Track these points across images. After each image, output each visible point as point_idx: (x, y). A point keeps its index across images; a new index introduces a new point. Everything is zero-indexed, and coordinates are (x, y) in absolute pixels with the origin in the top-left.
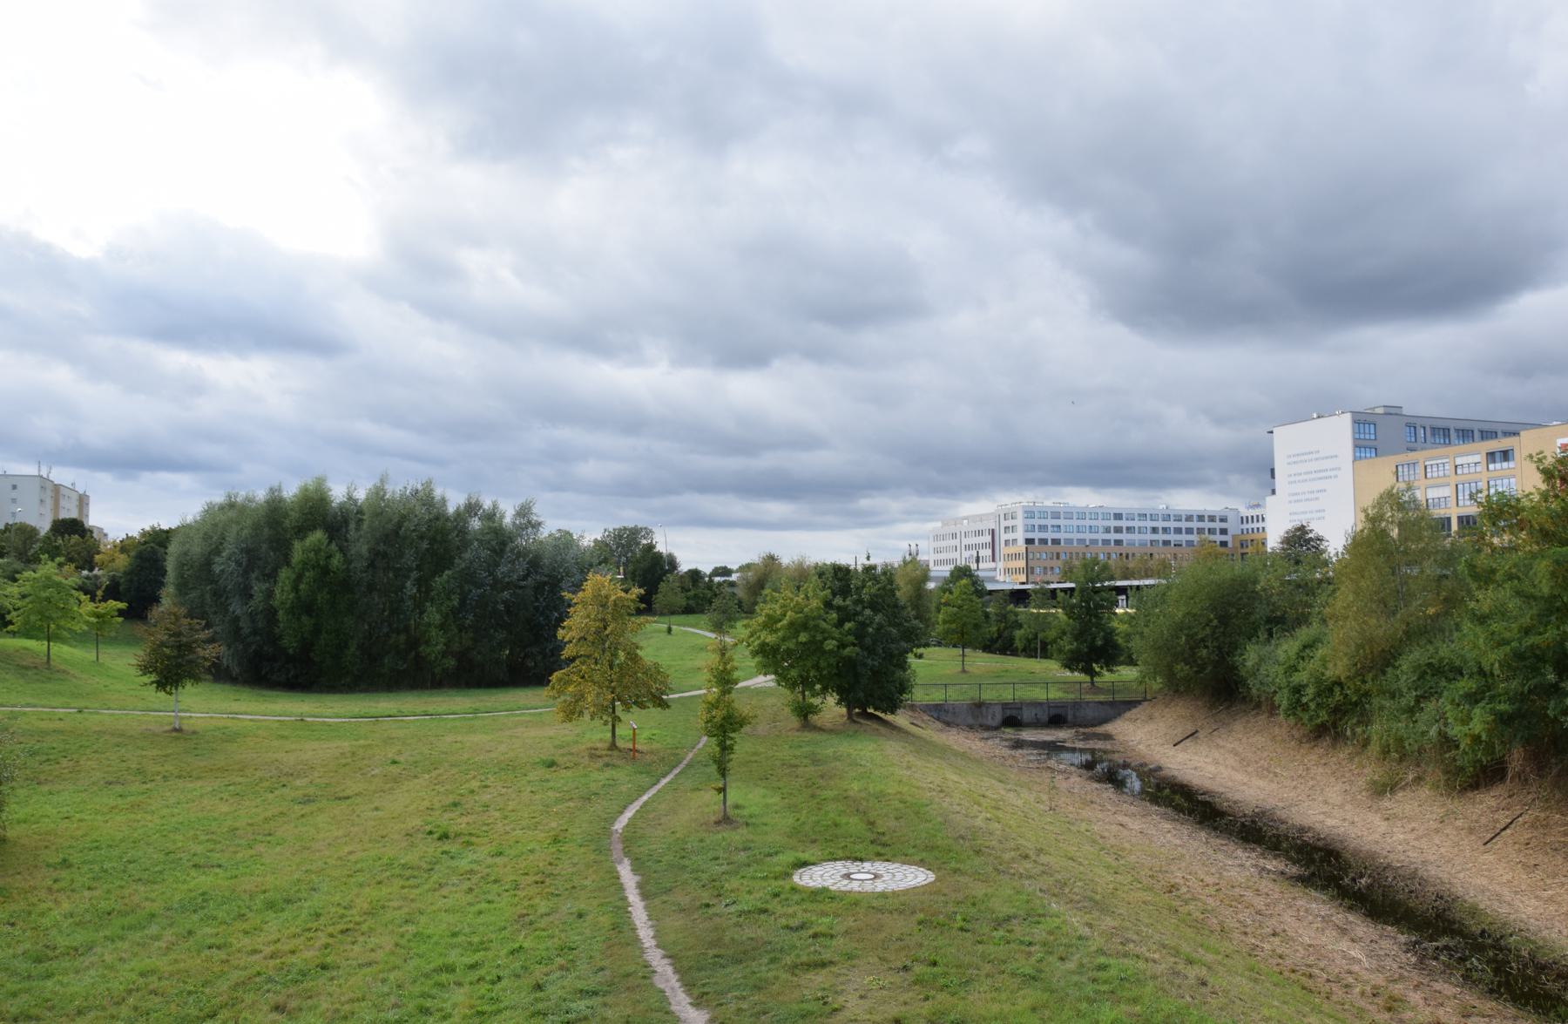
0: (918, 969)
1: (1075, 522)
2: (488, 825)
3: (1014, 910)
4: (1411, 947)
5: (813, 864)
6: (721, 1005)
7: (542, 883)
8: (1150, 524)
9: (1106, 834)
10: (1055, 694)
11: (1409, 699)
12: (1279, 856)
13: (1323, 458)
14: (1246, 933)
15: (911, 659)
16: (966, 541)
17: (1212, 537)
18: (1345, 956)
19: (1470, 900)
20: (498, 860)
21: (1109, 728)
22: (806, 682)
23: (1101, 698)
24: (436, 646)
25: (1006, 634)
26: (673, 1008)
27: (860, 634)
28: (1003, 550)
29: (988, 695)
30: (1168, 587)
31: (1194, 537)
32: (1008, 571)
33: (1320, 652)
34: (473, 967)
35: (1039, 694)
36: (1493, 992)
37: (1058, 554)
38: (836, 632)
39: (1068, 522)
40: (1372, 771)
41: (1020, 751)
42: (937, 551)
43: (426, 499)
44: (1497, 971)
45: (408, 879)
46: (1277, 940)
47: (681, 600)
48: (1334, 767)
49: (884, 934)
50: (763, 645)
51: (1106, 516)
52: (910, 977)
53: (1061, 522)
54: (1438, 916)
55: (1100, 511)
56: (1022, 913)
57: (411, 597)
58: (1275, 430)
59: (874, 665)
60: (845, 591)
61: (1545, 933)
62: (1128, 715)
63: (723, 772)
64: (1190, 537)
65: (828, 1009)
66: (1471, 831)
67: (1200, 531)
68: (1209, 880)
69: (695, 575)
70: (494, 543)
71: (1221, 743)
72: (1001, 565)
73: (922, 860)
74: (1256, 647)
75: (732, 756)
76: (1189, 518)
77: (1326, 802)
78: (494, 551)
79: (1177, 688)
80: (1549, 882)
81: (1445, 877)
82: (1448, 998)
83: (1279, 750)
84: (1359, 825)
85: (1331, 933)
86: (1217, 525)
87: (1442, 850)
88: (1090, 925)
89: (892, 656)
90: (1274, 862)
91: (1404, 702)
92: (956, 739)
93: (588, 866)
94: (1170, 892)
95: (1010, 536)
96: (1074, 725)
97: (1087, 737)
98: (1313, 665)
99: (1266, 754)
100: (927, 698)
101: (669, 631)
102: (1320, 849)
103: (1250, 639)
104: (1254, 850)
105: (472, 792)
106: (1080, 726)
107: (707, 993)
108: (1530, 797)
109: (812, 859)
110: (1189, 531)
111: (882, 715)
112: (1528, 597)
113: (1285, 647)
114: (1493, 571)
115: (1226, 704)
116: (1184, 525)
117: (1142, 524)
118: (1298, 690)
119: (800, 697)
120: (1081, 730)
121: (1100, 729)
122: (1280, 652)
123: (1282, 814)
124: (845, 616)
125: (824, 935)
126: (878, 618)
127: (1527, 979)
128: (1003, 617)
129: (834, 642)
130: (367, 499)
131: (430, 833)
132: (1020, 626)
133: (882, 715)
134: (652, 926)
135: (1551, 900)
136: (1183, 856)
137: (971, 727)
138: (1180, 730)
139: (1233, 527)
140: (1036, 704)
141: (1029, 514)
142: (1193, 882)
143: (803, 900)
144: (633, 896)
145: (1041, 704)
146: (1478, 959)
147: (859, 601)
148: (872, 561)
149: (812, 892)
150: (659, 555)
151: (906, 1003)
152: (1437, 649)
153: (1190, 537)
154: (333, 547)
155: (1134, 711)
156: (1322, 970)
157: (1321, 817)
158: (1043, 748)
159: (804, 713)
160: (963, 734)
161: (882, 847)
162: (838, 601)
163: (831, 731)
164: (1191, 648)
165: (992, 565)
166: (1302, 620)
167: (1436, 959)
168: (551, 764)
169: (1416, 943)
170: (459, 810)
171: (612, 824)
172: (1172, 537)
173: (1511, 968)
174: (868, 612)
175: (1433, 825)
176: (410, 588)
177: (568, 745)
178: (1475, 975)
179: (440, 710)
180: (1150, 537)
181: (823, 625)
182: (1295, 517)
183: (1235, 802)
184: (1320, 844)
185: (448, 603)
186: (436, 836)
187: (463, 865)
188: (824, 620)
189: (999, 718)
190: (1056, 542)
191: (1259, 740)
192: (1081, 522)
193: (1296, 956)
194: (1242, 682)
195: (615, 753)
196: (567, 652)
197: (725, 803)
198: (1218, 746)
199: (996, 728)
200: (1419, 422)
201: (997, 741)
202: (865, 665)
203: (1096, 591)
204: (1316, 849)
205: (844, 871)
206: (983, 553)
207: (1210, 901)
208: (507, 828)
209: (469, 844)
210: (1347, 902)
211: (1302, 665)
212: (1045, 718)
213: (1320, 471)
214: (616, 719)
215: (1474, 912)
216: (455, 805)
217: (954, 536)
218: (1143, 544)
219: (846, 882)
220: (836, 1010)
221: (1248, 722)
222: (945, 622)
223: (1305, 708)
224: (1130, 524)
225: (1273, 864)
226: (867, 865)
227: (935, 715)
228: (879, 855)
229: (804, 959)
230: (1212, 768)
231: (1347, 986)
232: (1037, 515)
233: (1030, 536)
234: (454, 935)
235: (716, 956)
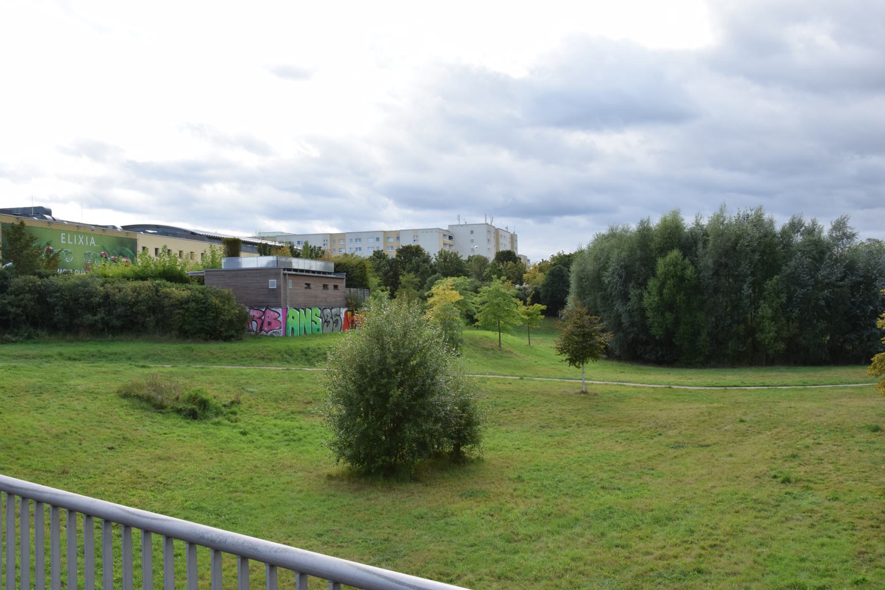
24: (769, 332)
57: (749, 296)
131: (775, 477)
154: (687, 261)
176: (747, 290)
185: (777, 300)
186: (779, 480)
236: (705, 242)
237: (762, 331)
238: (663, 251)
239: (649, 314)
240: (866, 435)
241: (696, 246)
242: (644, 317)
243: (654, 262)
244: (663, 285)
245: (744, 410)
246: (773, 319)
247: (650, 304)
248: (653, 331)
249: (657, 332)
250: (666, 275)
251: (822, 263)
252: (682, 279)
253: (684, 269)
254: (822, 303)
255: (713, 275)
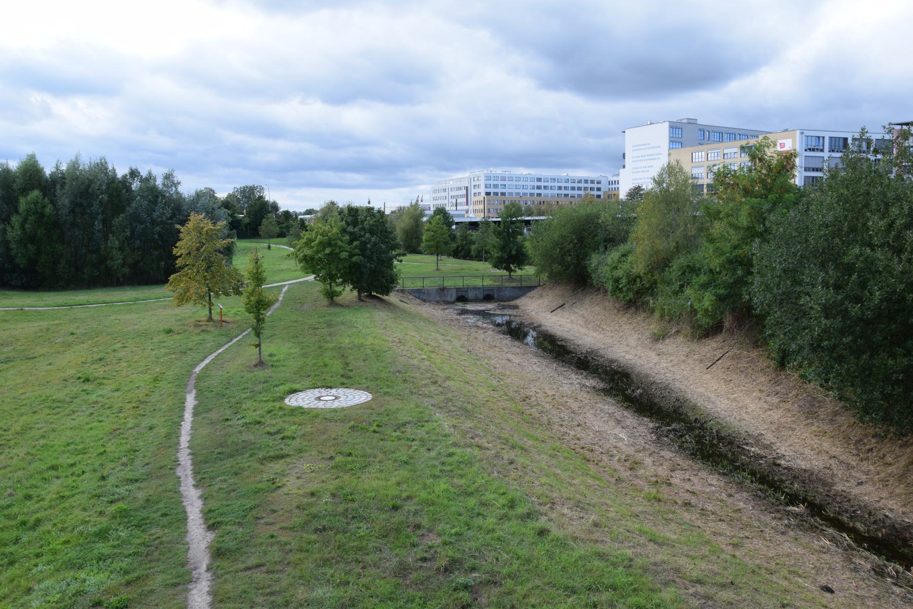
0: (339, 458)
1: (515, 183)
2: (117, 371)
3: (410, 418)
4: (655, 430)
5: (300, 391)
6: (210, 486)
7: (138, 407)
8: (557, 184)
9: (497, 366)
10: (487, 283)
11: (676, 287)
12: (595, 377)
13: (652, 148)
14: (562, 425)
15: (395, 262)
16: (451, 194)
17: (592, 193)
18: (616, 437)
19: (694, 401)
20: (116, 394)
21: (517, 302)
22: (332, 277)
23: (514, 284)
24: (117, 259)
25: (466, 248)
26: (181, 489)
27: (363, 248)
28: (473, 199)
29: (448, 283)
30: (553, 220)
31: (582, 192)
32: (475, 211)
33: (630, 258)
34: (72, 465)
35: (478, 283)
36: (693, 455)
37: (504, 201)
38: (348, 247)
39: (510, 183)
40: (654, 327)
41: (463, 316)
42: (435, 199)
43: (102, 167)
44: (697, 442)
45: (54, 409)
46: (579, 429)
47: (277, 230)
48: (635, 325)
49: (326, 436)
50: (305, 256)
51: (532, 180)
52: (331, 464)
53: (506, 183)
54: (674, 411)
55: (529, 176)
56: (414, 420)
57: (99, 231)
58: (626, 131)
59: (371, 268)
60: (355, 223)
61: (728, 418)
62: (529, 294)
63: (258, 334)
64: (580, 192)
65: (274, 486)
66: (701, 361)
67: (586, 189)
68: (550, 393)
69: (287, 214)
70: (150, 197)
71: (577, 311)
72: (471, 207)
73: (368, 387)
74: (597, 255)
75: (263, 325)
76: (580, 182)
77: (628, 345)
78: (150, 201)
79: (556, 279)
80: (735, 389)
81: (683, 387)
82: (666, 460)
83: (607, 315)
84: (643, 358)
85: (612, 423)
86: (595, 186)
87: (685, 372)
88: (454, 427)
89: (383, 261)
90: (591, 381)
91: (673, 287)
92: (427, 310)
93: (169, 396)
94: (525, 400)
95: (477, 191)
96: (500, 300)
97: (504, 307)
98: (625, 266)
99: (599, 317)
100: (413, 285)
101: (269, 247)
102: (620, 373)
103: (594, 251)
104: (581, 374)
105: (114, 351)
106: (501, 301)
107: (205, 478)
108: (734, 342)
109: (301, 388)
110: (579, 189)
111: (381, 296)
112: (736, 228)
113: (612, 256)
114: (719, 212)
115: (581, 289)
116: (576, 185)
117: (553, 184)
118: (617, 280)
119: (328, 287)
120: (502, 303)
121: (512, 303)
122: (609, 259)
123: (602, 352)
124: (354, 237)
125: (288, 437)
126: (373, 239)
127: (712, 445)
128: (465, 237)
129: (347, 253)
130: (68, 170)
131: (79, 378)
132: (474, 243)
133: (381, 296)
134: (191, 434)
135: (735, 400)
136: (539, 378)
137: (438, 302)
138: (555, 303)
139: (604, 187)
140: (476, 288)
141: (488, 178)
142: (541, 395)
143: (285, 415)
144: (188, 416)
145: (479, 288)
146: (690, 436)
147: (363, 229)
148: (371, 205)
149: (292, 410)
150: (266, 203)
151: (323, 482)
152: (693, 257)
153: (580, 192)
154: (46, 200)
155: (533, 292)
156: (600, 446)
157: (623, 354)
158: (477, 314)
159: (331, 295)
160: (432, 306)
161: (347, 380)
162: (350, 229)
163: (347, 306)
164: (562, 256)
165: (466, 207)
166: (624, 240)
167: (667, 436)
168: (169, 331)
169: (658, 427)
170: (102, 363)
171: (194, 368)
172: (570, 192)
173: (706, 440)
174: (367, 235)
175: (682, 358)
176: (98, 225)
177: (185, 319)
178: (686, 445)
179: (114, 299)
180: (557, 192)
181: (340, 243)
182: (635, 181)
183: (578, 346)
184: (620, 370)
185: (123, 234)
186: (82, 380)
187: (93, 398)
188: (341, 241)
189: (454, 297)
190: (503, 194)
191: (597, 309)
192: (517, 183)
193: (587, 438)
194: (589, 276)
195: (211, 323)
196: (179, 262)
197: (260, 353)
198: (575, 313)
199: (453, 303)
200: (706, 129)
201: (451, 310)
202: (366, 267)
203: (512, 223)
204: (617, 372)
205: (318, 395)
206: (459, 200)
207: (547, 406)
208: (129, 373)
209: (100, 384)
210: (626, 404)
211: (620, 265)
212: (481, 296)
213: (650, 155)
214: (211, 304)
215: (694, 408)
216: (101, 359)
217: (445, 190)
218: (553, 196)
219: (316, 402)
220: (279, 487)
221: (592, 299)
222: (427, 241)
223: (621, 290)
224: (546, 184)
225: (591, 382)
226: (334, 391)
227: (417, 296)
228: (343, 384)
229: (271, 454)
230: (569, 326)
231: (612, 456)
232: (492, 179)
233: (488, 190)
234: (68, 445)
235: (220, 453)
236: (63, 185)
237: (112, 259)
238: (25, 191)
239: (13, 246)
240: (163, 337)
241: (54, 188)
242: (8, 249)
243: (17, 201)
244: (25, 220)
245: (77, 325)
246: (121, 249)
247: (14, 238)
248: (17, 261)
249: (21, 261)
250: (28, 212)
251: (156, 205)
252: (42, 216)
253: (44, 207)
254: (156, 237)
255: (70, 212)
